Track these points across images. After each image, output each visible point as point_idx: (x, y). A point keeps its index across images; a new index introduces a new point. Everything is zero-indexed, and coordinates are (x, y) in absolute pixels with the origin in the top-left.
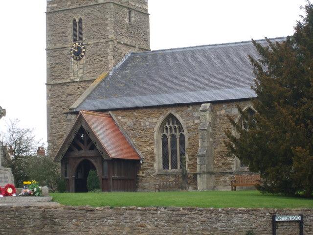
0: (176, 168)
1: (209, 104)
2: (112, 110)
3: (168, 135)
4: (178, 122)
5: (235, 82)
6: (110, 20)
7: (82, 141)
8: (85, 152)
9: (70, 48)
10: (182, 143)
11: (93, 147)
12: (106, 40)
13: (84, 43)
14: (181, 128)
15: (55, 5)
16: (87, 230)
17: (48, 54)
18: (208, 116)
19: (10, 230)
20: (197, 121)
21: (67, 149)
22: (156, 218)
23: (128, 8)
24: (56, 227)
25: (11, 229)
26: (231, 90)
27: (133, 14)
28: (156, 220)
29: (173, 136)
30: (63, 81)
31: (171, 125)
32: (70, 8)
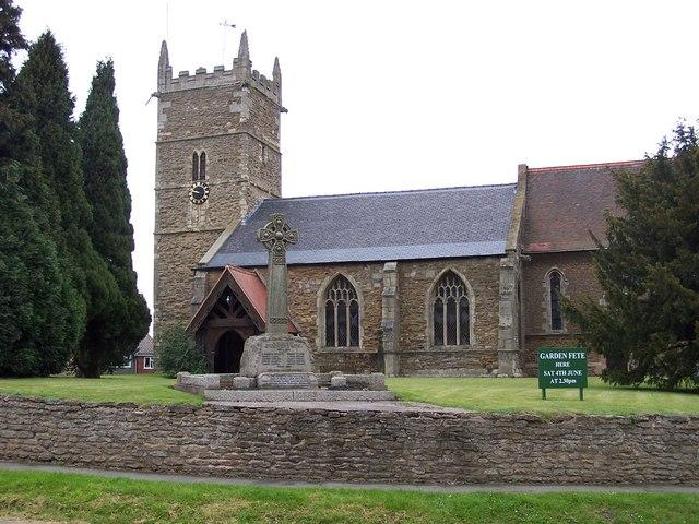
0: (345, 345)
1: (394, 264)
2: (256, 267)
3: (444, 300)
4: (349, 285)
5: (496, 234)
6: (244, 155)
7: (226, 306)
8: (231, 321)
10: (355, 312)
11: (242, 314)
14: (353, 294)
16: (529, 460)
17: (158, 196)
18: (394, 278)
19: (373, 460)
20: (378, 285)
21: (206, 315)
22: (649, 437)
23: (263, 143)
24: (468, 456)
25: (372, 457)
26: (405, 247)
29: (341, 303)
31: (339, 289)
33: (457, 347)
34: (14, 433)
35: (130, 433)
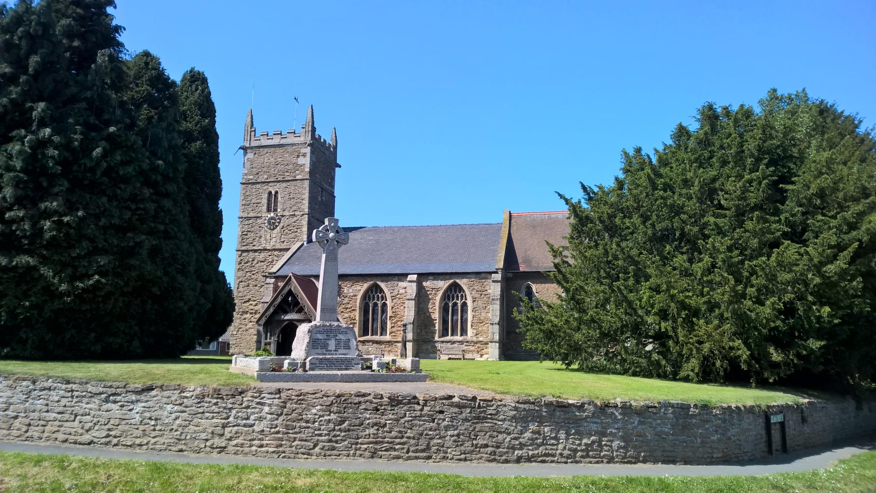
7: (289, 304)
9: (264, 218)
12: (302, 213)
13: (279, 215)
15: (252, 177)
23: (322, 188)
27: (324, 192)
28: (659, 425)
30: (255, 248)
32: (267, 180)
33: (458, 338)
34: (55, 415)
35: (174, 416)
